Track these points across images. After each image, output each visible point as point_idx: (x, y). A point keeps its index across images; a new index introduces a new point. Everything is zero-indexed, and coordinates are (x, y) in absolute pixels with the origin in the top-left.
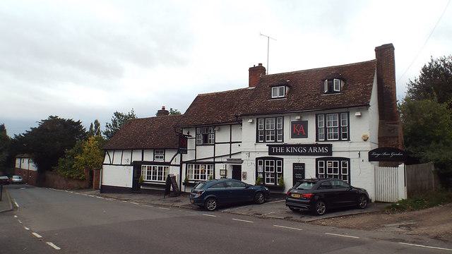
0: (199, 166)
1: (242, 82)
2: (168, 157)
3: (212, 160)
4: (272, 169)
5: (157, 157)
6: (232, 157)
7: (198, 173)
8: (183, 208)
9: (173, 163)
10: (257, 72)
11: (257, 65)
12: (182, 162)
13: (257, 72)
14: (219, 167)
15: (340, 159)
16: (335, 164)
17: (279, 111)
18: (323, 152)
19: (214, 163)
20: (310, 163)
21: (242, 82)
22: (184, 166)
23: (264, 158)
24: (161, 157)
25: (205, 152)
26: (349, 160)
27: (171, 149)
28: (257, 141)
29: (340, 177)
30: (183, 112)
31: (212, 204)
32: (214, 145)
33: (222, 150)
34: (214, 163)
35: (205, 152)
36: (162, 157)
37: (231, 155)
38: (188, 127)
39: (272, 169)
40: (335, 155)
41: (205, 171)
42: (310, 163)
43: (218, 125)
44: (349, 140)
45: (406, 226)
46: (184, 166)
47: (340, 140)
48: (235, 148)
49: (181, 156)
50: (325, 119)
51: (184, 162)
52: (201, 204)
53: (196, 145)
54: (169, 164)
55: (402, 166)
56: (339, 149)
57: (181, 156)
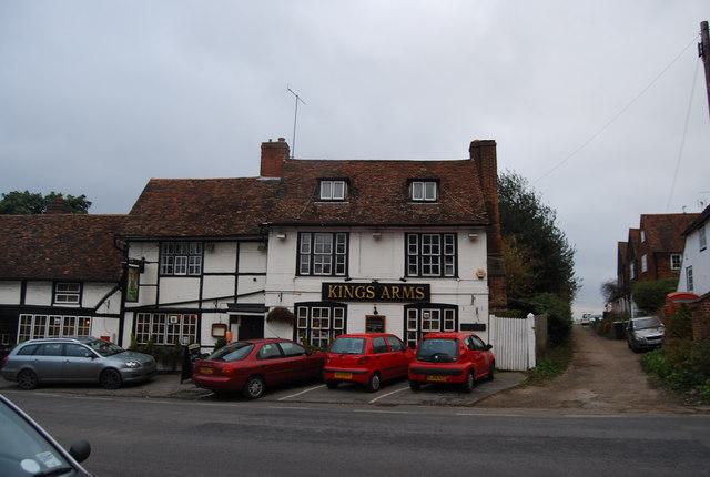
0: (147, 317)
1: (248, 166)
2: (90, 299)
3: (196, 306)
4: (325, 323)
5: (60, 298)
6: (240, 301)
7: (162, 331)
8: (172, 396)
9: (101, 310)
10: (274, 152)
11: (275, 140)
12: (124, 310)
13: (274, 152)
14: (208, 320)
15: (442, 306)
16: (435, 315)
17: (343, 226)
18: (415, 299)
19: (199, 312)
20: (394, 317)
21: (250, 167)
22: (129, 318)
23: (310, 304)
24: (71, 298)
25: (178, 290)
26: (456, 307)
27: (97, 281)
28: (298, 274)
29: (331, 332)
30: (627, 241)
31: (255, 387)
32: (201, 277)
33: (219, 287)
34: (199, 312)
35: (178, 290)
36: (75, 298)
37: (236, 297)
38: (144, 240)
39: (325, 323)
40: (434, 300)
41: (177, 327)
42: (394, 317)
43: (210, 243)
44: (456, 276)
45: (502, 391)
46: (129, 318)
47: (443, 276)
48: (246, 285)
49: (201, 296)
50: (334, 240)
51: (130, 310)
52: (231, 388)
53: (159, 276)
54: (92, 312)
55: (531, 315)
56: (441, 290)
57: (201, 296)
